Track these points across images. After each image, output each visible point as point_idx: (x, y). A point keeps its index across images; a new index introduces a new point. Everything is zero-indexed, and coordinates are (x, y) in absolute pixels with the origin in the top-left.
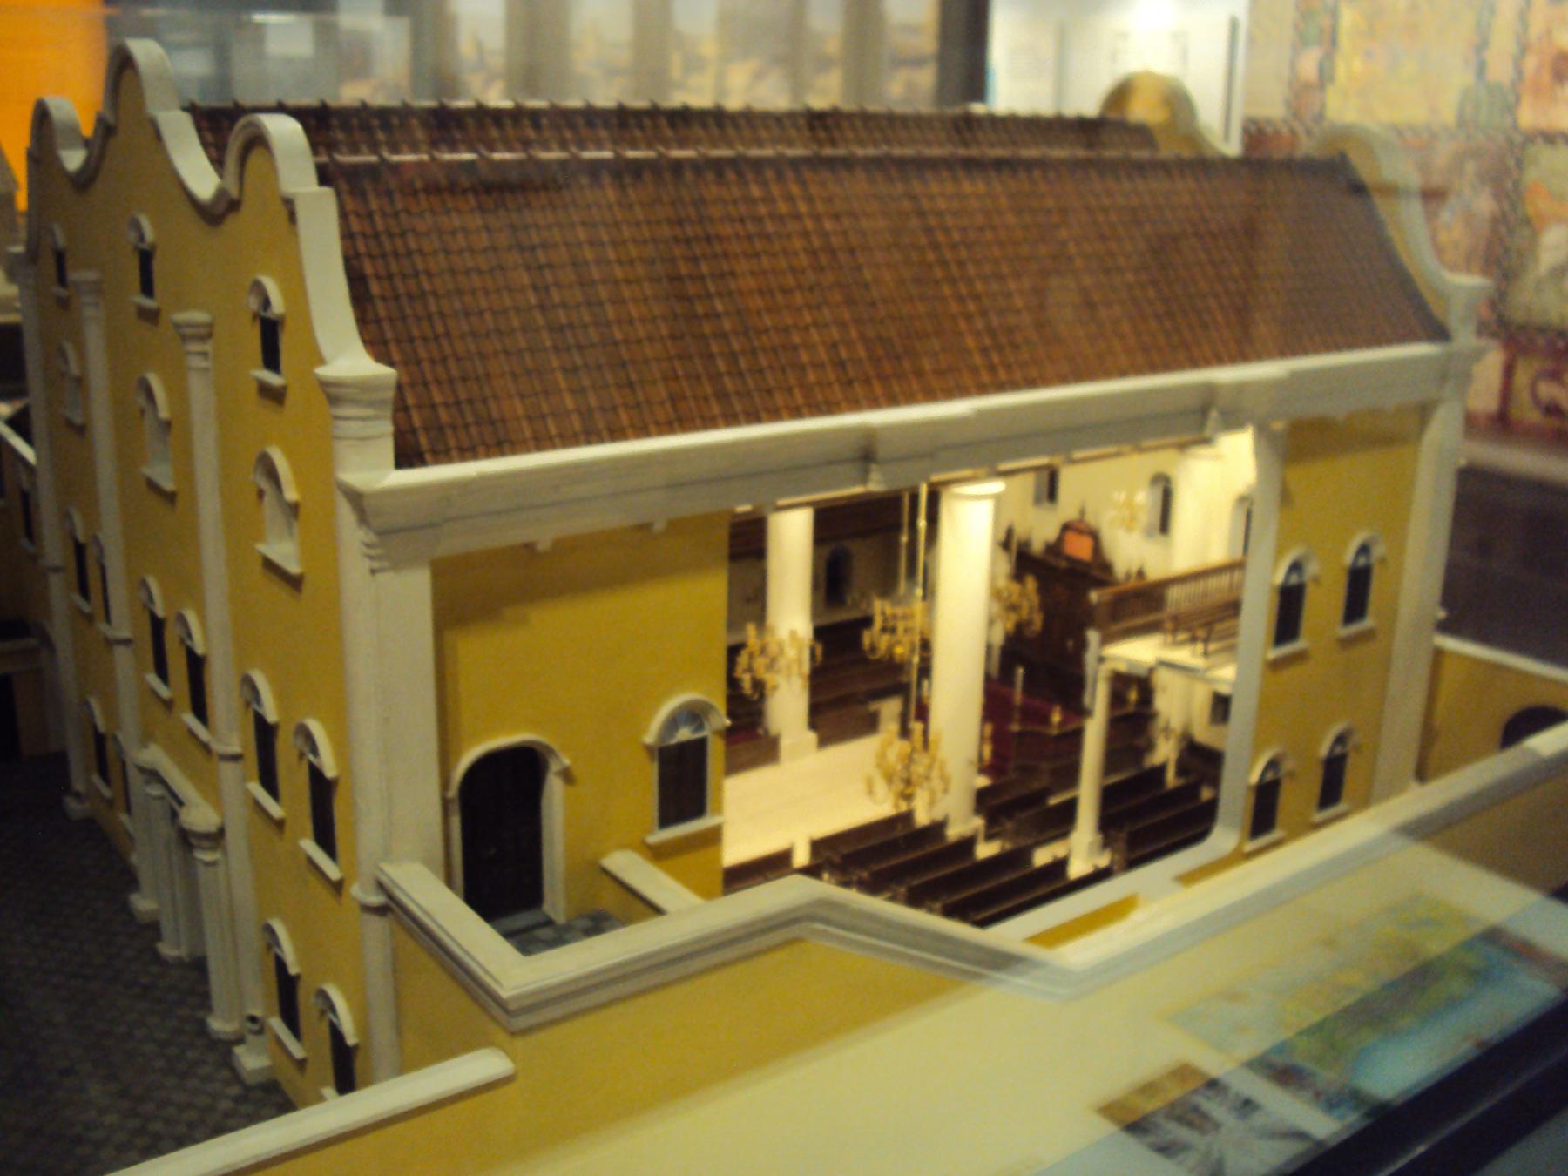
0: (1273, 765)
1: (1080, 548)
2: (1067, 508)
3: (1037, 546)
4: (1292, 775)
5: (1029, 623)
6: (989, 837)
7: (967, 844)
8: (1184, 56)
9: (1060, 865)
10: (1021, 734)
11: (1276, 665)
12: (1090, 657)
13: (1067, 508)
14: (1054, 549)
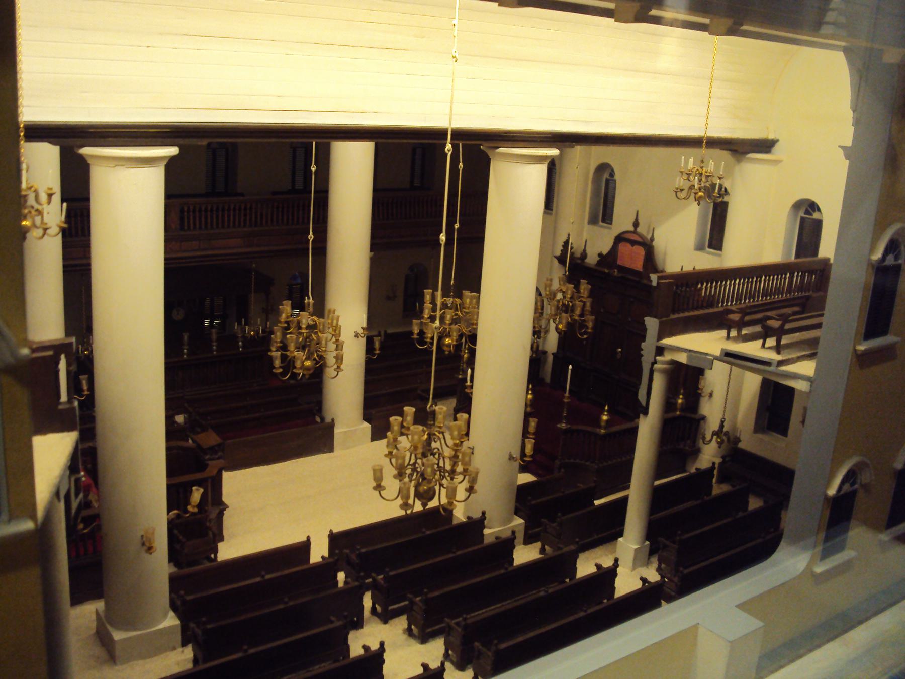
0: (850, 477)
1: (632, 258)
2: (622, 222)
3: (592, 259)
4: (865, 487)
5: (583, 325)
6: (529, 540)
7: (506, 546)
8: (636, 224)
9: (607, 576)
10: (566, 431)
11: (863, 360)
12: (648, 347)
13: (622, 222)
14: (608, 259)
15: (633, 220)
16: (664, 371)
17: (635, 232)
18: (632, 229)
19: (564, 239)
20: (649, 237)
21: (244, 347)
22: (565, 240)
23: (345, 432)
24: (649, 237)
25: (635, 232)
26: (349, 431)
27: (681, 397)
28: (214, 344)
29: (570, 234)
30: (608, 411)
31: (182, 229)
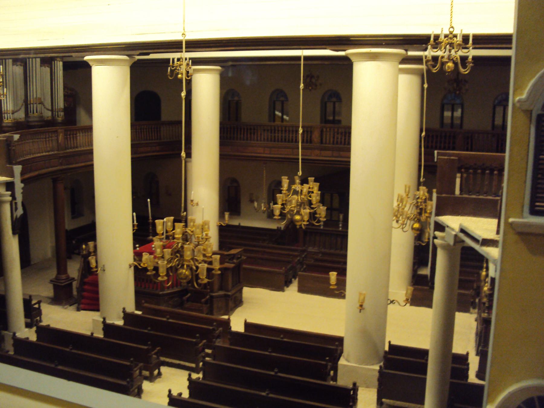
16: (446, 248)
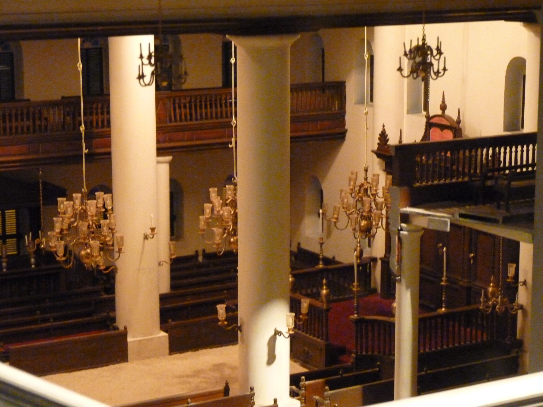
15: (440, 102)
17: (443, 116)
18: (440, 112)
19: (379, 131)
20: (455, 118)
21: (37, 264)
22: (380, 132)
23: (140, 341)
24: (455, 118)
25: (443, 116)
26: (143, 340)
27: (491, 285)
28: (4, 260)
29: (385, 125)
30: (326, 285)
31: (171, 121)
